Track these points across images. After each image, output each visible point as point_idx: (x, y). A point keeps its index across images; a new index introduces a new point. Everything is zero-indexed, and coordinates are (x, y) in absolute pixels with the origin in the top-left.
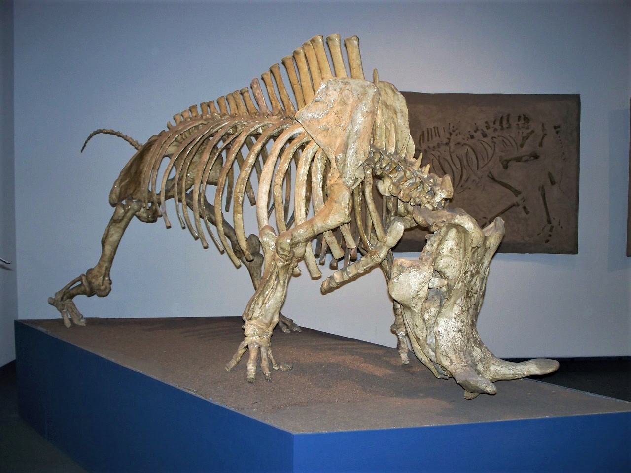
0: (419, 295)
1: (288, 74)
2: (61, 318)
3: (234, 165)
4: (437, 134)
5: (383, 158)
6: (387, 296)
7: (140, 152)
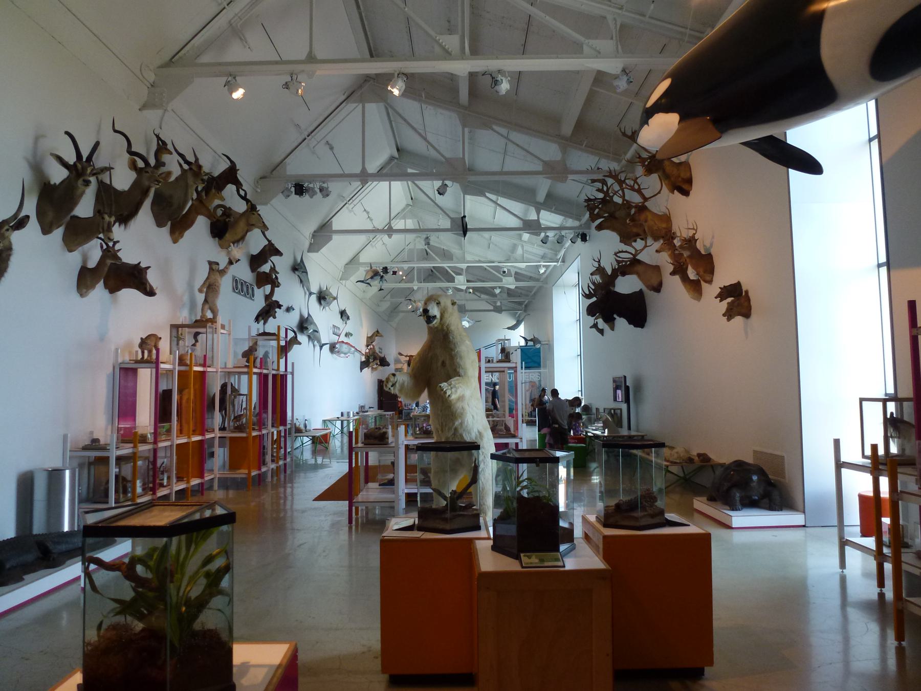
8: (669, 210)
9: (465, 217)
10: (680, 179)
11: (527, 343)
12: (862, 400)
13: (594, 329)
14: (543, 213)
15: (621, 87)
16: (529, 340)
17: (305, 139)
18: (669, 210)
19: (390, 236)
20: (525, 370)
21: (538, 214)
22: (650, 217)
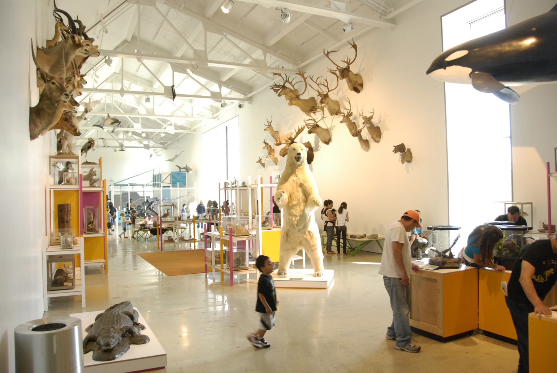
0: (73, 78)
1: (29, 70)
2: (219, 91)
3: (452, 244)
4: (74, 66)
5: (89, 224)
6: (53, 15)
7: (113, 93)
8: (349, 99)
9: (173, 86)
10: (357, 84)
11: (180, 170)
12: (531, 204)
13: (259, 164)
14: (223, 88)
15: (348, 30)
16: (182, 168)
17: (100, 21)
18: (349, 99)
19: (122, 95)
20: (163, 190)
21: (220, 88)
22: (330, 102)
